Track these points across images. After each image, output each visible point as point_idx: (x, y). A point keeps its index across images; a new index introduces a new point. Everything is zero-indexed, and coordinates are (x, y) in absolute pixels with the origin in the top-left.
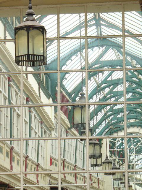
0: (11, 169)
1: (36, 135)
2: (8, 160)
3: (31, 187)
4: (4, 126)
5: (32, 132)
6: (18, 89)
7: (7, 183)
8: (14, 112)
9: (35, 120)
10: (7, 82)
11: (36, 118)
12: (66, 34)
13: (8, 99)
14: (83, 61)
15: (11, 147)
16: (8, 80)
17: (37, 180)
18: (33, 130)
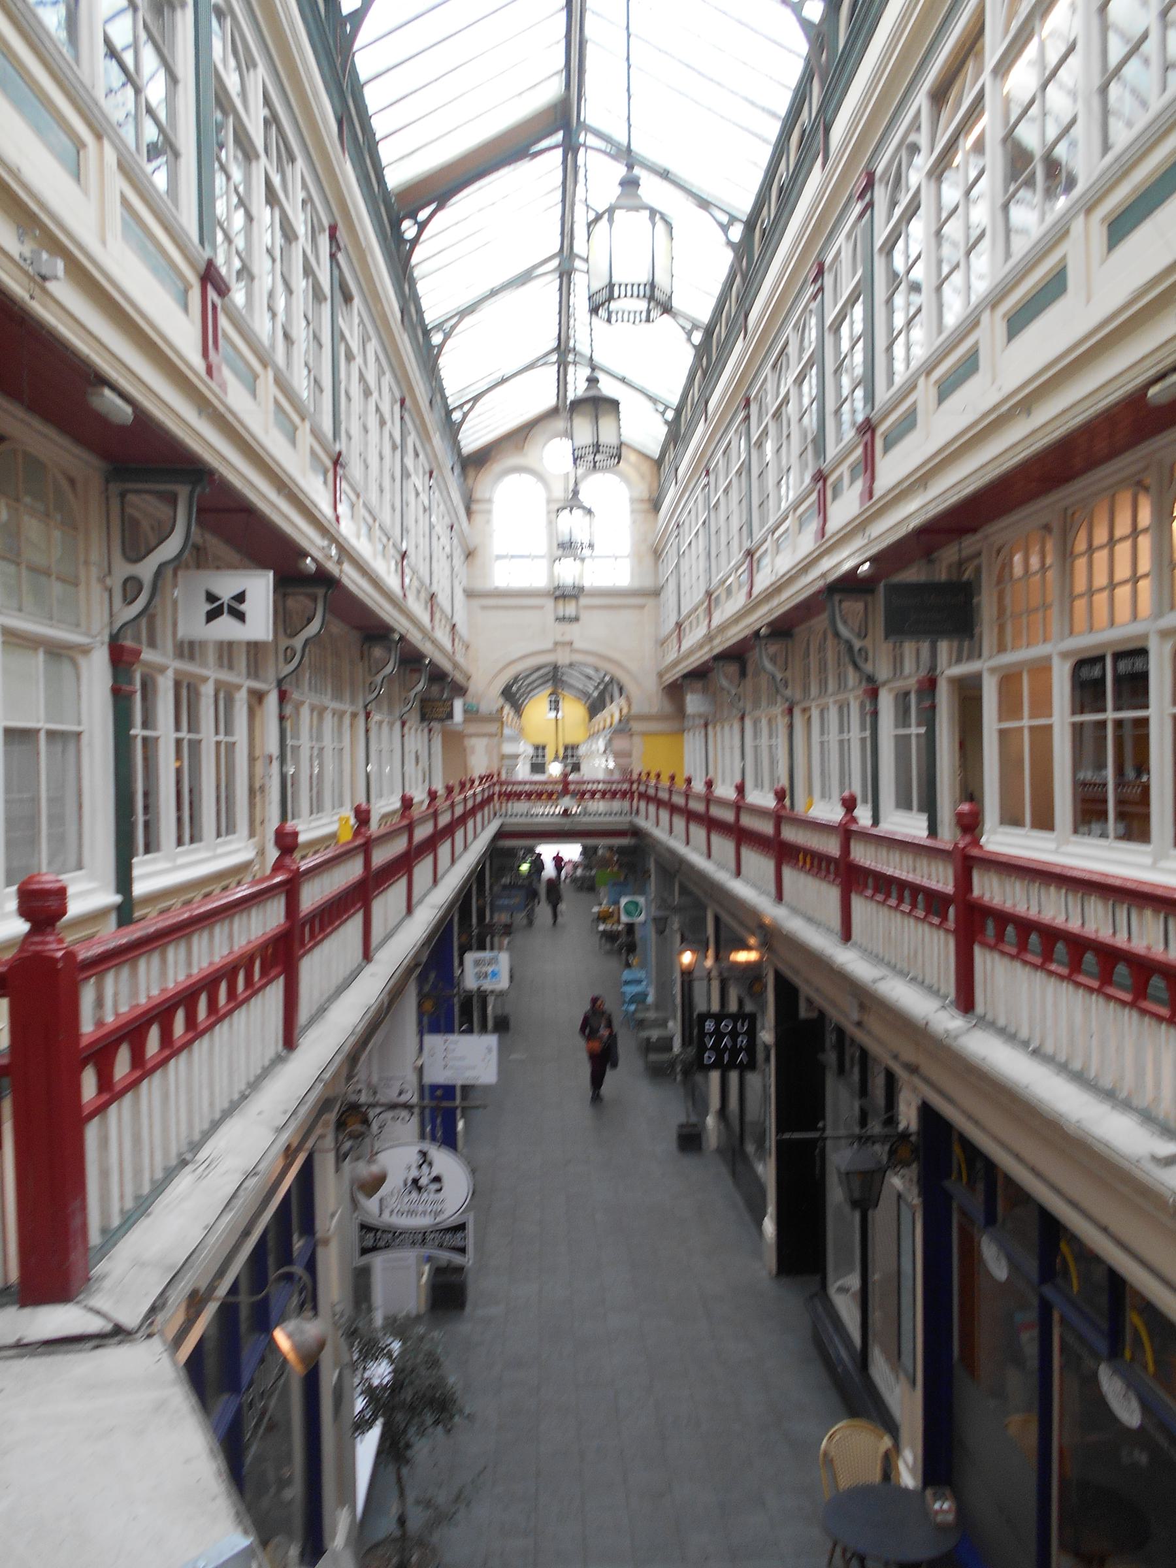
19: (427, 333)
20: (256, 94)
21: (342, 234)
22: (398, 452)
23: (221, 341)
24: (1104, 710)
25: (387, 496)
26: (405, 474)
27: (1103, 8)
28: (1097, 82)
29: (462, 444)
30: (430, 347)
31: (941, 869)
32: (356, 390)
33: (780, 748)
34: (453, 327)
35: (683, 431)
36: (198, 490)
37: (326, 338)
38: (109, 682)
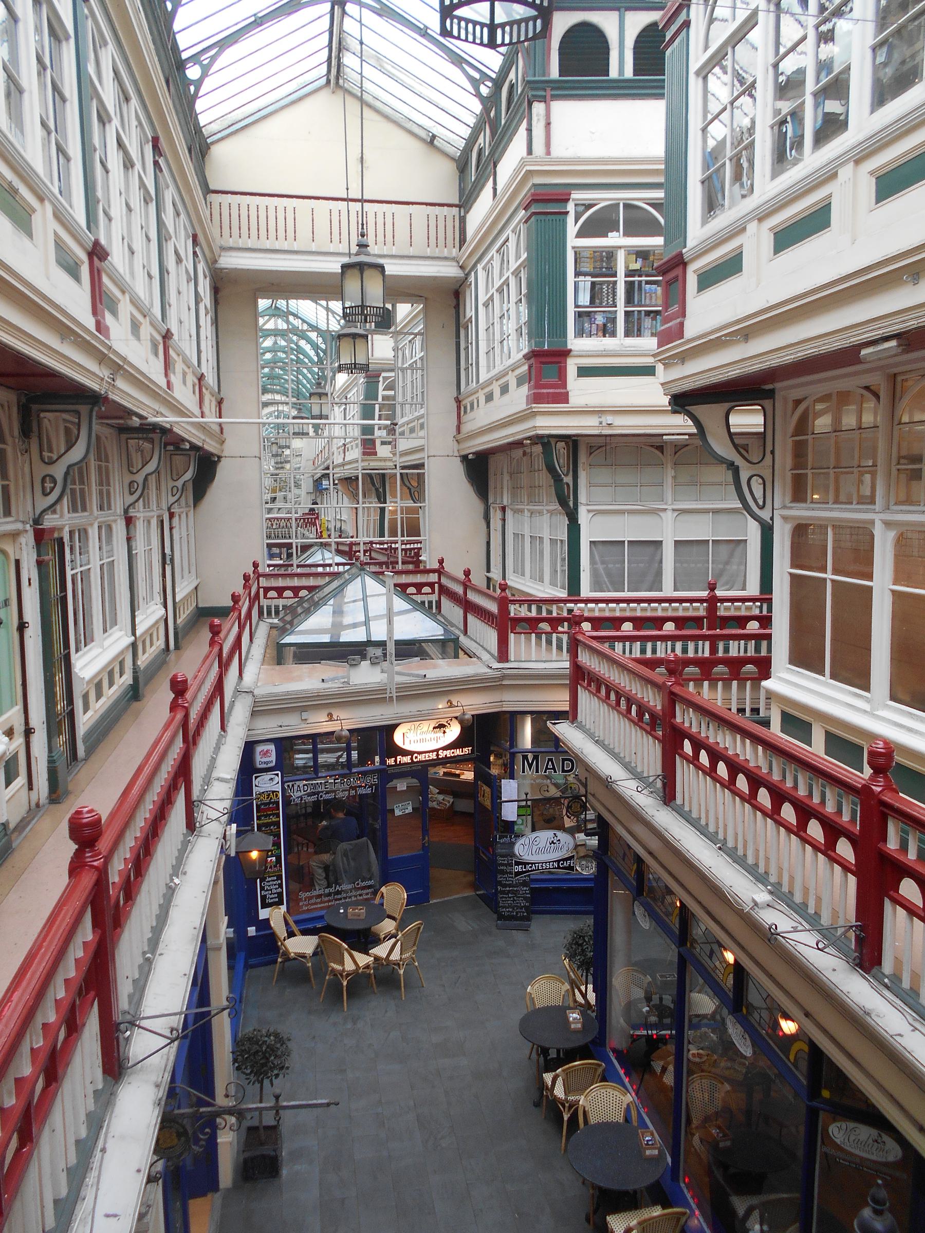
0: (169, 387)
1: (188, 282)
2: (159, 364)
3: (182, 424)
4: (141, 260)
5: (166, 246)
6: (130, 75)
7: (200, 444)
8: (166, 240)
9: (177, 219)
10: (190, 242)
11: (178, 214)
12: (255, 21)
13: (72, 41)
14: (305, 327)
15: (199, 376)
16: (153, 146)
17: (165, 380)
18: (169, 242)
19: (181, 65)
20: (107, 69)
21: (163, 143)
22: (152, 207)
23: (104, 297)
24: (76, 489)
25: (139, 259)
26: (163, 236)
27: (778, 5)
28: (772, 60)
29: (203, 120)
30: (187, 82)
31: (616, 672)
32: (115, 160)
33: (880, 440)
34: (213, 59)
35: (503, 122)
36: (96, 409)
37: (70, 88)
38: (35, 557)
